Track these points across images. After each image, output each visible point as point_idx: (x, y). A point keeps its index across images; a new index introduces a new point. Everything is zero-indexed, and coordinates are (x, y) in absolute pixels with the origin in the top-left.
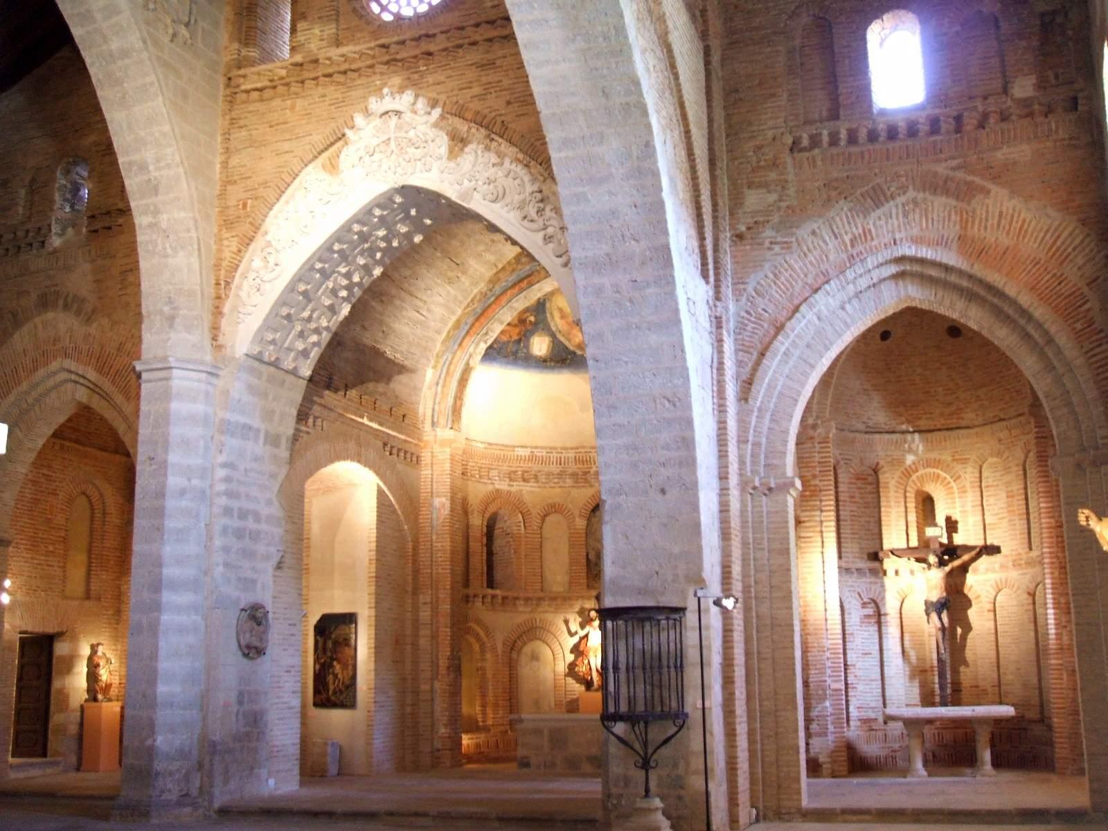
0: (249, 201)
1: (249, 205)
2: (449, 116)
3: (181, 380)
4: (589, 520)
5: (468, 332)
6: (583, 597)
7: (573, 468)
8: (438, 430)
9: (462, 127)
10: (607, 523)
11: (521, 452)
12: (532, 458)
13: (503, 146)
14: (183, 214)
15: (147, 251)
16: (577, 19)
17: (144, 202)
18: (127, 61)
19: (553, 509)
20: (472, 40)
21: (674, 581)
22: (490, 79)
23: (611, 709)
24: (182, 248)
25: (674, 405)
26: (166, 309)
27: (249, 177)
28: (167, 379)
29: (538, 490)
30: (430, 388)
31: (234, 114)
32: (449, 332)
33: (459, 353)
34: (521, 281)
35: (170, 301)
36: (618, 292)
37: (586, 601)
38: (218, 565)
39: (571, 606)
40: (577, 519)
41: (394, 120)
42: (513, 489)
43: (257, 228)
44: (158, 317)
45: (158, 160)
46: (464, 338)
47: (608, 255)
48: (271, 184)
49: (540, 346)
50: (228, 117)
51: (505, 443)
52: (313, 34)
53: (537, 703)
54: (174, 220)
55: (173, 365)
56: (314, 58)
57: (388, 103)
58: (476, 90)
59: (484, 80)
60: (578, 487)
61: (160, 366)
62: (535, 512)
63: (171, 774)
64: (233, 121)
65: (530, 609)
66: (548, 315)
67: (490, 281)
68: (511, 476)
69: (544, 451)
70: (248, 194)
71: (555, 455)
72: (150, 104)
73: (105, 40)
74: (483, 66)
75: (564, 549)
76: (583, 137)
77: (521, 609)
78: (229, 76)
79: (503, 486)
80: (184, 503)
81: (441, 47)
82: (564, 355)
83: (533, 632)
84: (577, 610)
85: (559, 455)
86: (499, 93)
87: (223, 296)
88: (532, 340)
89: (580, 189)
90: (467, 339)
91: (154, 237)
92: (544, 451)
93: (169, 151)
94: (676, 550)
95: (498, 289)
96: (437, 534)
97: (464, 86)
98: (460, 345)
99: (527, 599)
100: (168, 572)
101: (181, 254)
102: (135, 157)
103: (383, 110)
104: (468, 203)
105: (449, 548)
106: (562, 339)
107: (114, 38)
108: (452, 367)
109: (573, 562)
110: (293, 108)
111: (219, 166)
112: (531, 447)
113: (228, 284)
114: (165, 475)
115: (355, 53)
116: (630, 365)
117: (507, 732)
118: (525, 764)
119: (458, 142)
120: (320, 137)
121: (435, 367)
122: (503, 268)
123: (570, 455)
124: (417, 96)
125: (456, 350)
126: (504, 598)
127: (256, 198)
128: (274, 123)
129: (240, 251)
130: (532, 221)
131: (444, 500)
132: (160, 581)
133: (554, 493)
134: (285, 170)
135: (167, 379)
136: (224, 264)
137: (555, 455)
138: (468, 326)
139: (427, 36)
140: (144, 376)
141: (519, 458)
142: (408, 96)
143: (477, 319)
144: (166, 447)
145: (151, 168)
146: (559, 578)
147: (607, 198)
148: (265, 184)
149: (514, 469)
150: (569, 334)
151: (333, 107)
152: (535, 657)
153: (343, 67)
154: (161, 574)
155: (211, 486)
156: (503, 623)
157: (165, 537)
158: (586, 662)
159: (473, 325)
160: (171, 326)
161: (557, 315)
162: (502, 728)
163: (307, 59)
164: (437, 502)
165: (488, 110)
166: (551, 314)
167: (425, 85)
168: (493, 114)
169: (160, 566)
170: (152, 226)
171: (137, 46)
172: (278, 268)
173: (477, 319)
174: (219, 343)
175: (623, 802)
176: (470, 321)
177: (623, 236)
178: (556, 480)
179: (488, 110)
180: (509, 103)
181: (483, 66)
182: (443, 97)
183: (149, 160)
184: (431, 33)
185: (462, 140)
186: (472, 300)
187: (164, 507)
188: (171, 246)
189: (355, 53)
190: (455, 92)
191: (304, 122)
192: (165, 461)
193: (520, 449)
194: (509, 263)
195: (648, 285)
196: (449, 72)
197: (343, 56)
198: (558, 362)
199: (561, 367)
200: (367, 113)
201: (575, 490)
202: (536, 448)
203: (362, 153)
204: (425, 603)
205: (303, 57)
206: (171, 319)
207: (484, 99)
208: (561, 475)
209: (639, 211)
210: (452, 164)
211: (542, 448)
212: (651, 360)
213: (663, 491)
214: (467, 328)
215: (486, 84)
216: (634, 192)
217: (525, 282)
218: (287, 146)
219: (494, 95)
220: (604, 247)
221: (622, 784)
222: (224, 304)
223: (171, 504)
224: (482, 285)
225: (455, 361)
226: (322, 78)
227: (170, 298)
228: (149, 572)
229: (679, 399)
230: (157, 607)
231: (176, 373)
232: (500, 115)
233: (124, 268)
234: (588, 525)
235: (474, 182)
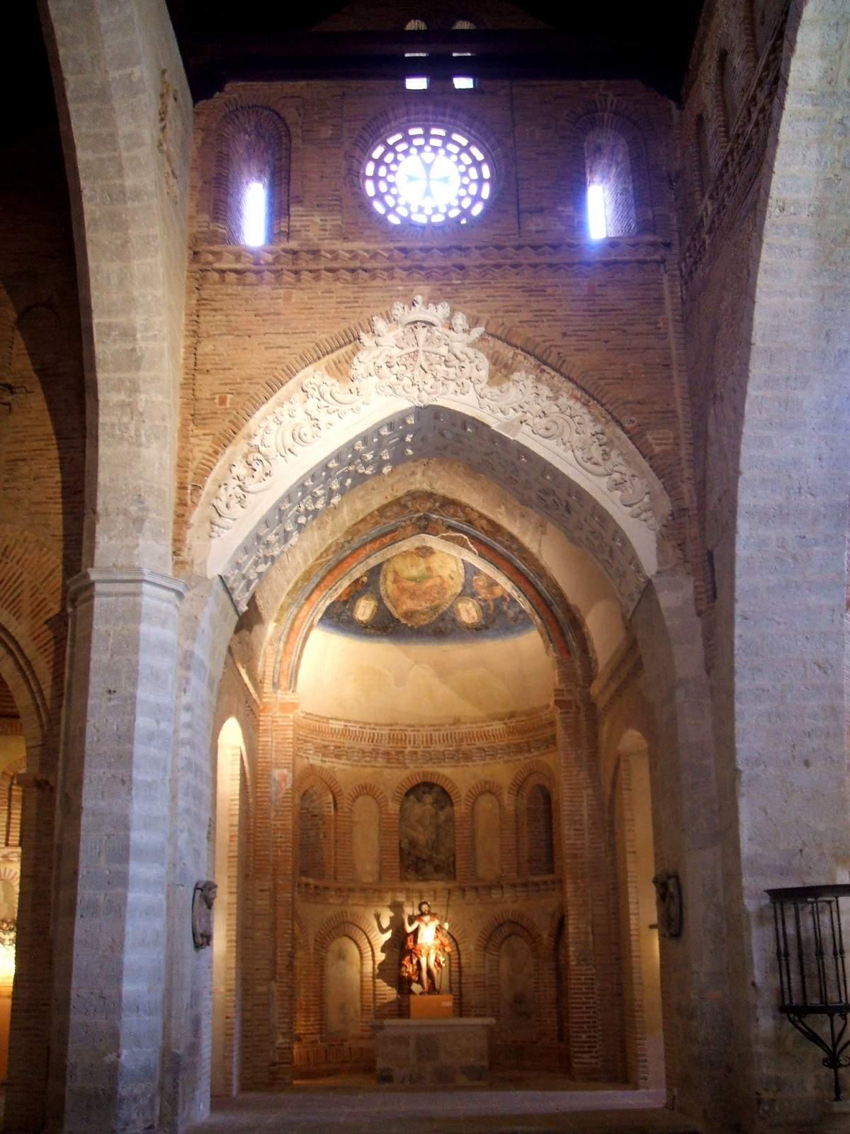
0: (229, 396)
1: (228, 401)
2: (490, 338)
3: (153, 598)
4: (402, 805)
5: (318, 585)
6: (394, 890)
7: (385, 746)
8: (279, 691)
9: (508, 352)
10: (743, 795)
11: (336, 725)
12: (345, 733)
13: (556, 379)
14: (160, 398)
15: (113, 436)
16: (831, 253)
17: (117, 375)
18: (136, 204)
19: (365, 790)
20: (513, 262)
21: (820, 860)
22: (542, 306)
23: (787, 1002)
24: (157, 438)
25: (825, 672)
26: (133, 509)
27: (230, 369)
28: (135, 594)
29: (348, 768)
30: (271, 644)
31: (204, 294)
32: (296, 583)
33: (306, 607)
34: (385, 535)
35: (140, 499)
36: (783, 547)
37: (398, 894)
38: (182, 831)
39: (382, 899)
40: (390, 803)
41: (422, 333)
42: (327, 765)
43: (236, 427)
44: (121, 518)
45: (147, 329)
46: (313, 591)
47: (780, 506)
48: (259, 380)
49: (364, 610)
50: (195, 296)
51: (323, 715)
52: (312, 221)
53: (342, 1007)
54: (152, 402)
55: (146, 578)
56: (315, 248)
57: (419, 313)
58: (525, 316)
59: (535, 306)
60: (391, 768)
61: (126, 577)
62: (347, 791)
63: (135, 1099)
64: (201, 301)
65: (340, 901)
66: (381, 578)
67: (347, 532)
68: (323, 750)
69: (358, 726)
70: (227, 389)
71: (369, 731)
72: (149, 260)
73: (120, 172)
74: (531, 291)
75: (374, 834)
76: (788, 378)
77: (331, 901)
78: (196, 250)
79: (316, 761)
80: (152, 751)
81: (478, 263)
82: (386, 621)
83: (344, 927)
84: (389, 903)
85: (372, 731)
86: (551, 323)
87: (189, 502)
88: (358, 603)
89: (767, 433)
90: (317, 593)
91: (125, 419)
92: (358, 726)
93: (158, 320)
94: (821, 827)
95: (356, 542)
96: (276, 811)
97: (510, 308)
98: (308, 599)
99: (339, 890)
100: (138, 836)
101: (154, 445)
102: (121, 319)
103: (412, 318)
104: (514, 435)
105: (290, 827)
106: (389, 605)
107: (130, 174)
108: (297, 624)
109: (383, 850)
110: (288, 298)
111: (183, 350)
112: (346, 721)
113: (197, 488)
114: (133, 713)
115: (367, 251)
116: (782, 627)
117: (316, 1041)
118: (386, 1078)
119: (501, 370)
120: (325, 336)
121: (277, 621)
122: (364, 520)
123: (383, 732)
124: (453, 311)
125: (303, 604)
126: (316, 887)
127: (239, 394)
128: (260, 312)
129: (216, 452)
130: (595, 464)
131: (285, 771)
132: (126, 848)
133: (365, 772)
134: (279, 367)
135: (135, 594)
136: (193, 465)
137: (369, 731)
138: (319, 579)
139: (460, 248)
140: (98, 587)
141: (334, 732)
142: (443, 310)
143: (330, 572)
144: (134, 681)
145: (139, 336)
146: (368, 867)
147: (792, 446)
148: (250, 379)
149: (327, 743)
150: (398, 600)
151: (343, 306)
152: (342, 956)
153: (352, 265)
154: (128, 838)
155: (176, 731)
156: (316, 914)
157: (133, 792)
158: (415, 961)
159: (323, 578)
160: (140, 531)
161: (390, 577)
162: (313, 1037)
163: (306, 248)
164: (277, 773)
165: (541, 339)
166: (385, 576)
167: (462, 300)
168: (548, 344)
169: (127, 828)
170: (122, 405)
171: (149, 188)
172: (268, 478)
173: (330, 572)
174: (181, 558)
175: (777, 1109)
176: (321, 573)
177: (800, 488)
178: (368, 759)
179: (541, 339)
180: (564, 335)
181: (531, 291)
182: (486, 316)
183: (138, 327)
184: (464, 246)
185: (506, 366)
186: (327, 550)
187: (131, 754)
188: (145, 434)
189: (367, 251)
190: (500, 314)
191: (303, 316)
192: (133, 697)
193: (334, 722)
194: (371, 514)
195: (816, 543)
196: (491, 291)
197: (350, 252)
198: (379, 630)
199: (381, 635)
200: (388, 318)
201: (388, 771)
202: (349, 721)
203: (381, 362)
204: (262, 891)
205: (301, 245)
206: (139, 521)
207: (536, 327)
208: (375, 752)
209: (823, 464)
210: (495, 390)
211: (356, 722)
212: (807, 622)
213: (807, 763)
214: (316, 580)
215: (537, 311)
216: (823, 444)
217: (389, 537)
218: (281, 340)
219: (546, 324)
220: (778, 497)
221: (774, 1088)
222: (191, 513)
223: (139, 750)
224: (339, 535)
225: (301, 616)
226: (323, 272)
227: (140, 496)
228: (109, 836)
229: (832, 666)
230: (122, 880)
231: (146, 588)
232: (556, 346)
233: (11, 457)
234: (400, 810)
235: (520, 414)
